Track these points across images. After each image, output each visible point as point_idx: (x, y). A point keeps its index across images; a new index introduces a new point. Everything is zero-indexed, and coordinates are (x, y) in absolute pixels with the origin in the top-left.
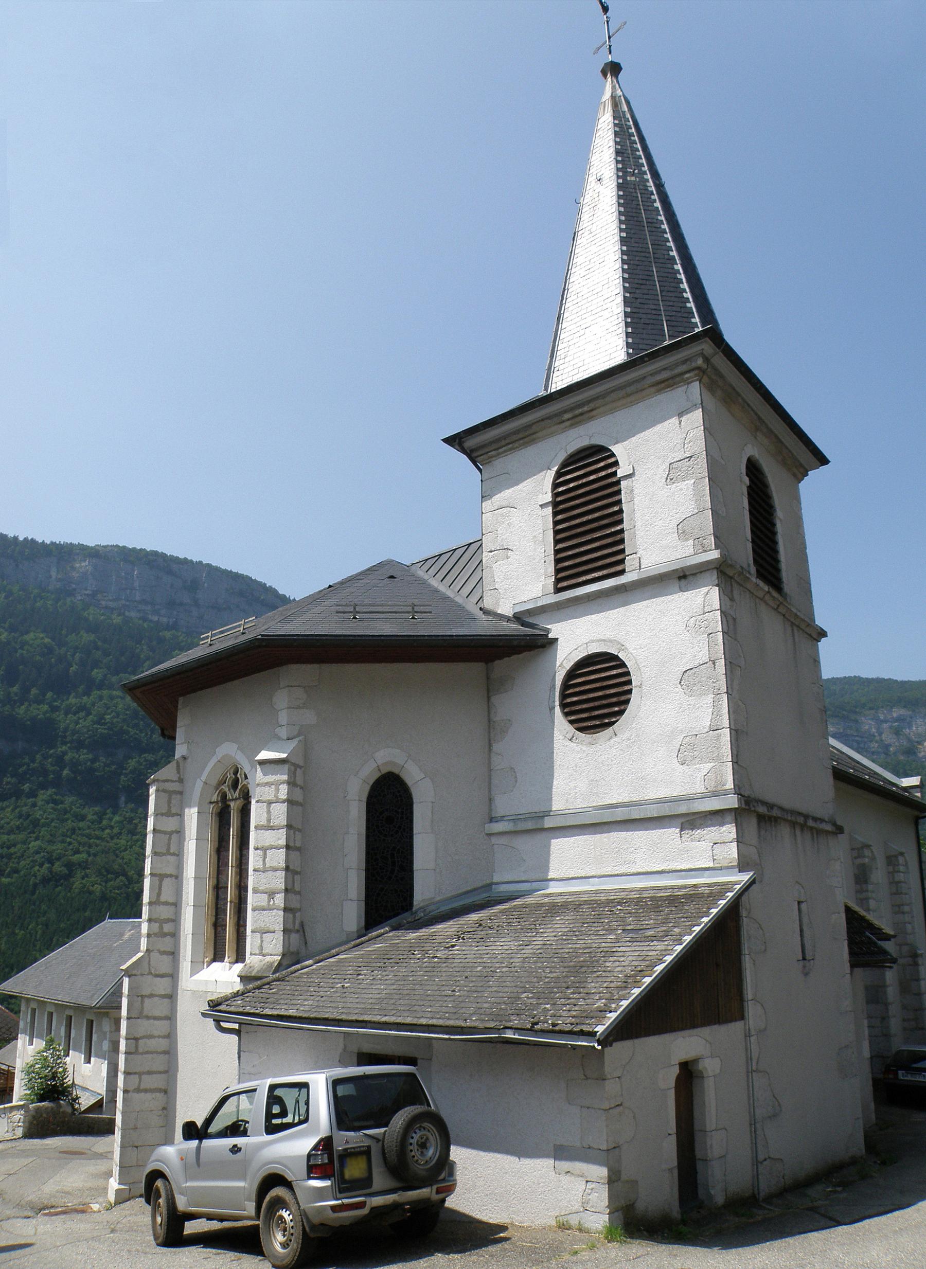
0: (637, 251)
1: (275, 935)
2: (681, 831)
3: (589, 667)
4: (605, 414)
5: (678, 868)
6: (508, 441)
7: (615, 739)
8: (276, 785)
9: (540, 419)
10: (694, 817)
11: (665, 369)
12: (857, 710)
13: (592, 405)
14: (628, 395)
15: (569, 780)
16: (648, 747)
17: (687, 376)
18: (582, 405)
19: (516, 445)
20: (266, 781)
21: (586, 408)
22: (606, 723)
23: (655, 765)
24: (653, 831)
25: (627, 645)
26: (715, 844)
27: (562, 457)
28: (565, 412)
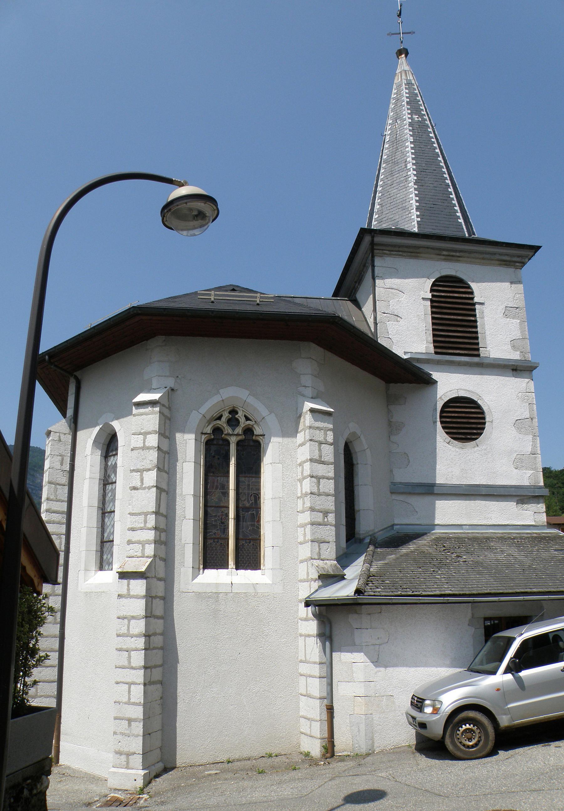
0: (439, 179)
1: (330, 545)
2: (517, 504)
3: (457, 404)
4: (467, 262)
5: (516, 524)
6: (400, 249)
7: (476, 448)
8: (325, 431)
9: (426, 246)
10: (524, 498)
11: (507, 255)
12: (35, 469)
13: (461, 254)
14: (483, 259)
15: (448, 467)
16: (497, 456)
17: (518, 264)
18: (456, 251)
19: (404, 254)
20: (316, 426)
21: (458, 254)
22: (469, 438)
23: (502, 467)
24: (502, 503)
25: (483, 397)
26: (535, 513)
27: (438, 275)
28: (444, 250)
